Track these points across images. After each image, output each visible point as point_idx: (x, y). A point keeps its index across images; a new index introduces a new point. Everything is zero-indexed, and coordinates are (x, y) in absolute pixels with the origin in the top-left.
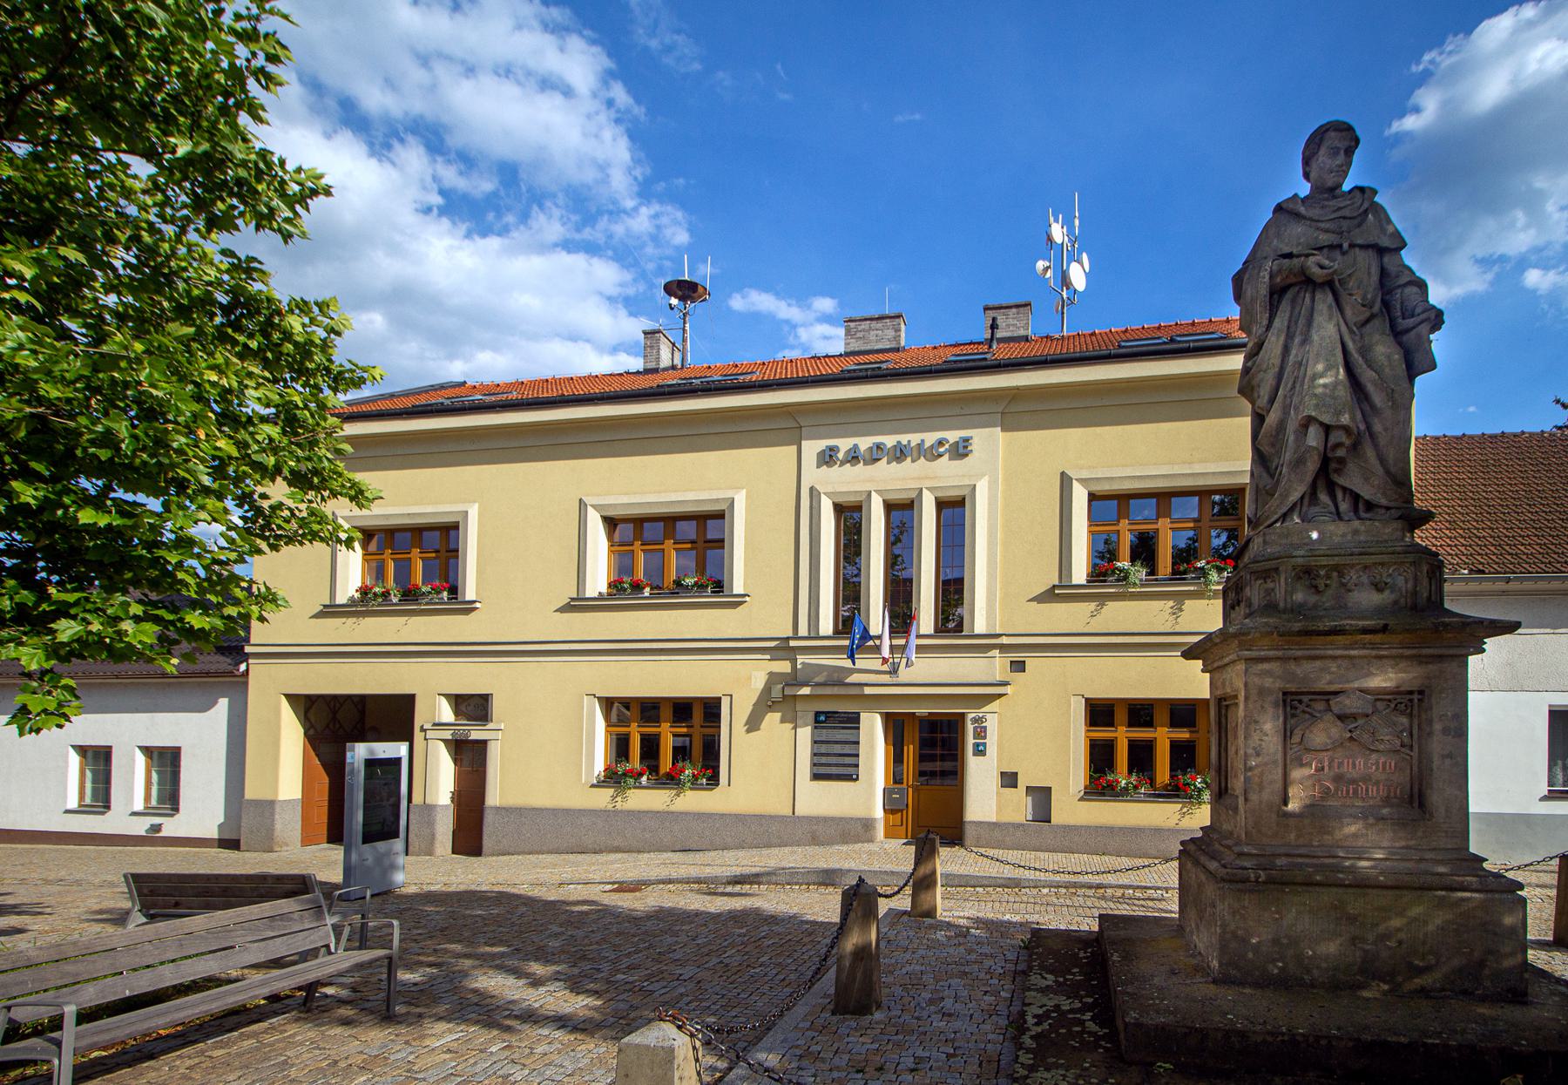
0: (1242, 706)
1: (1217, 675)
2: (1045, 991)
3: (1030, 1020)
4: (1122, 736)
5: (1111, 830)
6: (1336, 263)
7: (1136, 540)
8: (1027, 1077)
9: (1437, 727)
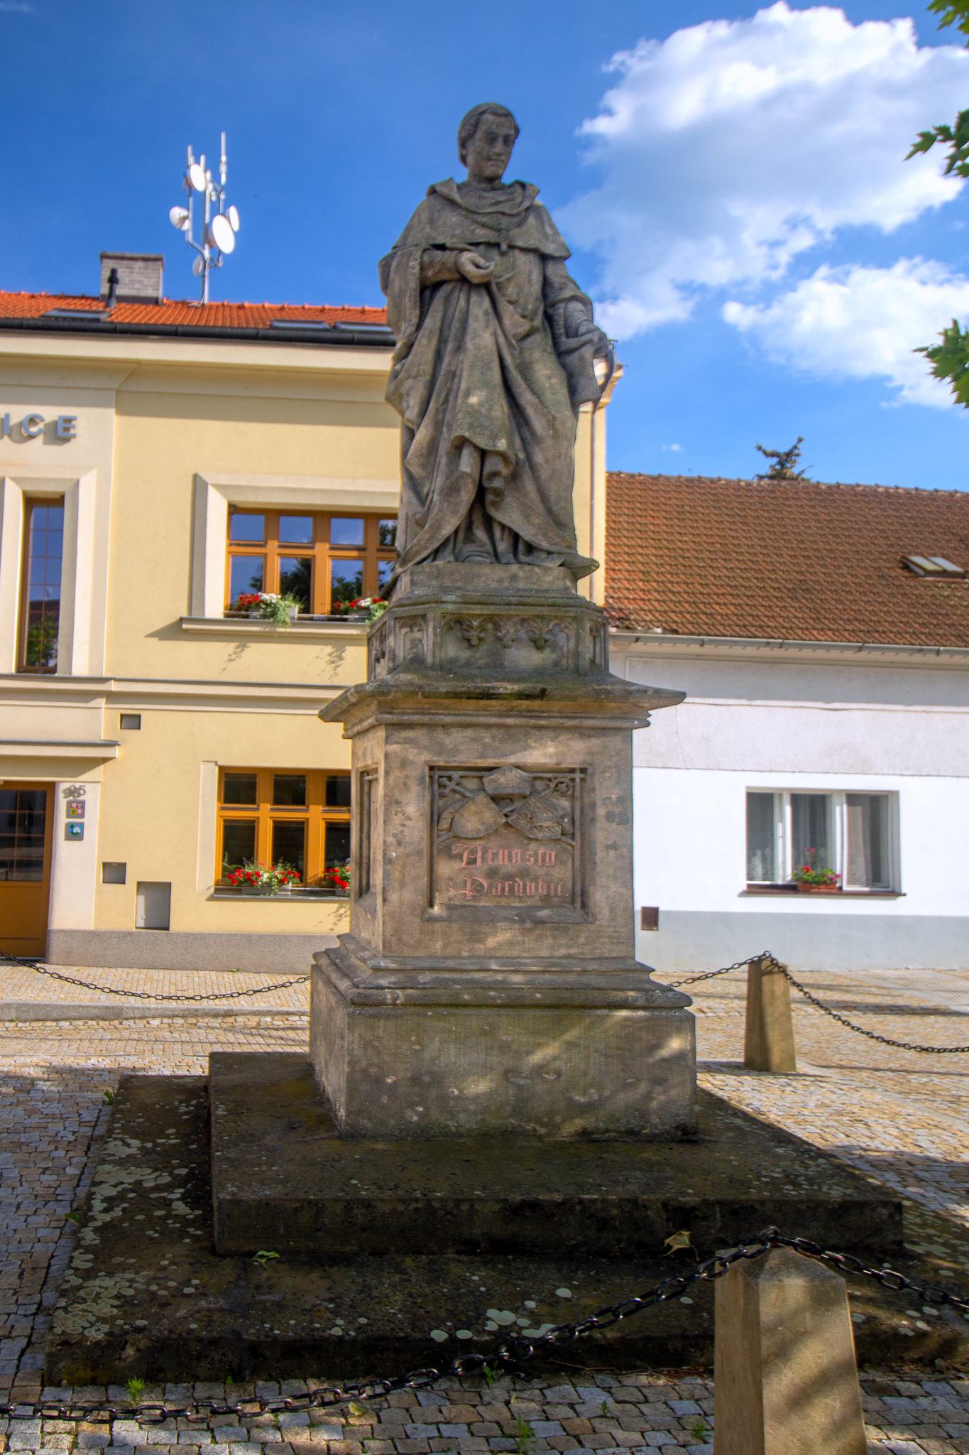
0: (381, 781)
1: (359, 743)
2: (122, 1163)
3: (98, 1205)
4: (265, 816)
5: (248, 939)
6: (493, 265)
7: (288, 566)
8: (80, 1288)
9: (601, 811)
